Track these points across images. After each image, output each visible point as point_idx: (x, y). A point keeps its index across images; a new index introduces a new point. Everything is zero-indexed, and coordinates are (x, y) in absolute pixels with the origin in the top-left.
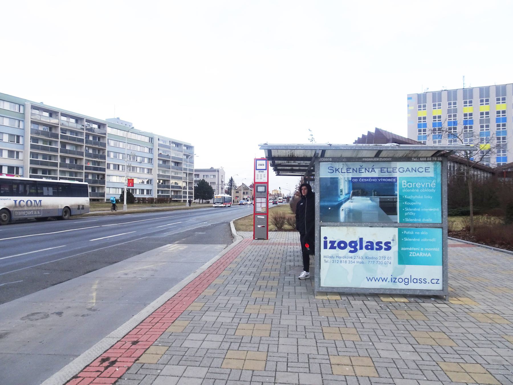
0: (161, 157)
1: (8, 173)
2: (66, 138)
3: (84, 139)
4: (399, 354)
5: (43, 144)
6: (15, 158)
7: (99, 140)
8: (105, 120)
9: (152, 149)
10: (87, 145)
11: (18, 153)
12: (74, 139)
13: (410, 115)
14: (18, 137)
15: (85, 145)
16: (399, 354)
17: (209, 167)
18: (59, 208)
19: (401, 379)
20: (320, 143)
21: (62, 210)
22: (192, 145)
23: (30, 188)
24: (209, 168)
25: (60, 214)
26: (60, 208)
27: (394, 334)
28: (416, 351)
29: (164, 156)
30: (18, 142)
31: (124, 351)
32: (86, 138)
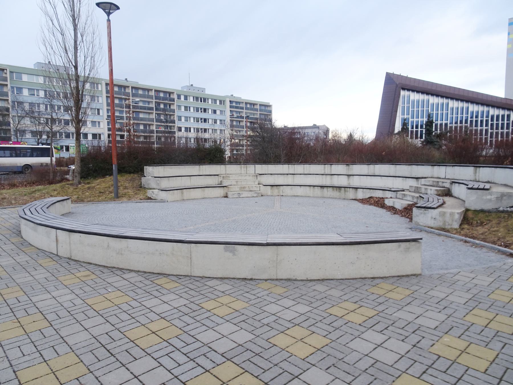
0: (248, 119)
1: (93, 139)
2: (137, 107)
3: (153, 107)
4: (217, 315)
5: (119, 114)
6: (97, 127)
7: (170, 107)
8: (180, 89)
9: (224, 111)
10: (156, 112)
11: (99, 122)
12: (144, 108)
13: (510, 46)
14: (98, 110)
15: (154, 112)
16: (217, 315)
17: (311, 125)
18: (18, 165)
19: (119, 327)
20: (248, 99)
21: (21, 168)
22: (271, 104)
23: (250, 150)
24: (312, 125)
25: (20, 170)
26: (19, 165)
27: (62, 282)
28: (149, 308)
29: (252, 118)
30: (99, 114)
31: (376, 304)
32: (155, 106)
